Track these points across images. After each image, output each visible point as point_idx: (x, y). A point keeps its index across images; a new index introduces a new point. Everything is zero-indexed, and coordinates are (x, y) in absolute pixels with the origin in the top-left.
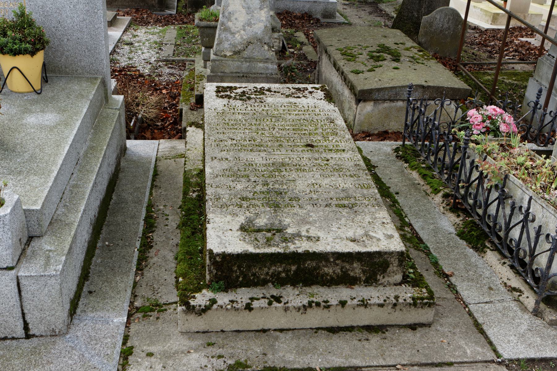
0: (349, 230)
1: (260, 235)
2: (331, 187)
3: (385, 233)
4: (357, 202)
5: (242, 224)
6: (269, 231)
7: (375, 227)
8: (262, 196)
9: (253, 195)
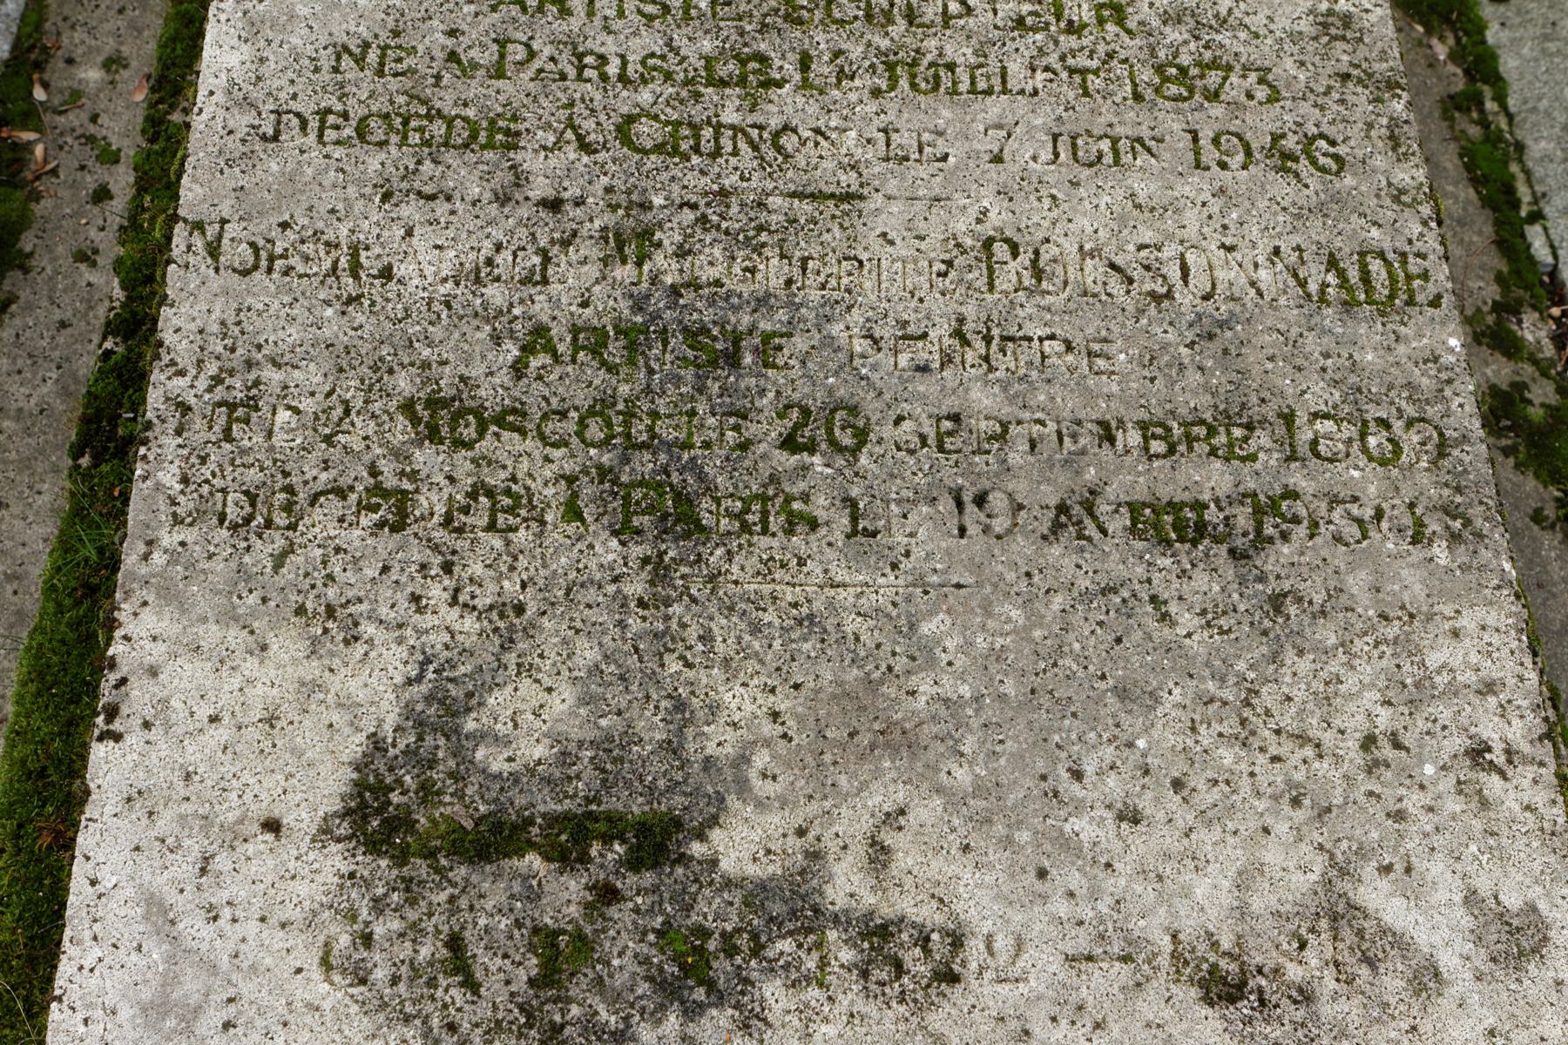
0: (1205, 838)
1: (490, 900)
2: (1116, 286)
3: (1484, 885)
4: (1297, 478)
5: (377, 744)
6: (569, 841)
7: (1414, 802)
8: (579, 383)
9: (518, 369)
